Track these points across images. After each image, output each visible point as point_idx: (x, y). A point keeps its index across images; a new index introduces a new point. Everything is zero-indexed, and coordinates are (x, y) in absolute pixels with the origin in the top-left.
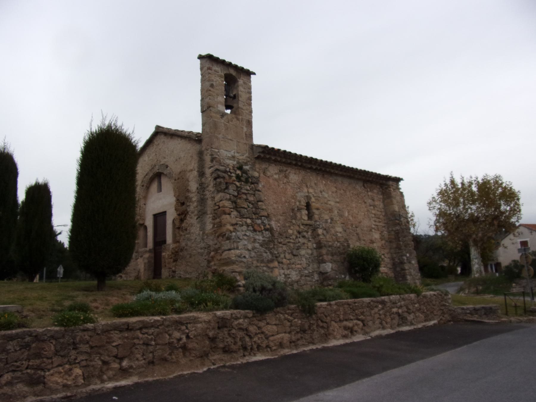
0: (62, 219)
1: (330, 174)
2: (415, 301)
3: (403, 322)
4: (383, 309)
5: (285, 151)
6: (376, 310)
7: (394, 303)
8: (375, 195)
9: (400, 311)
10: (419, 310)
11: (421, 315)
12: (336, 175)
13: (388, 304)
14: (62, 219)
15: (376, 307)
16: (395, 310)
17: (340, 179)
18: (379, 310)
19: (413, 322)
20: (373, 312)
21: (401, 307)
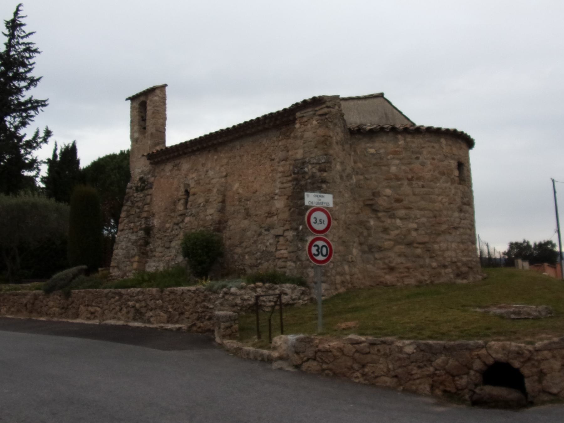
0: (302, 336)
1: (224, 144)
2: (157, 296)
3: (140, 318)
4: (119, 300)
5: (234, 127)
6: (113, 300)
7: (131, 296)
8: (380, 99)
9: (137, 305)
10: (161, 307)
11: (162, 314)
12: (231, 141)
13: (125, 297)
14: (302, 336)
15: (114, 298)
16: (131, 303)
17: (237, 144)
18: (116, 301)
19: (152, 319)
20: (110, 302)
21: (138, 301)
